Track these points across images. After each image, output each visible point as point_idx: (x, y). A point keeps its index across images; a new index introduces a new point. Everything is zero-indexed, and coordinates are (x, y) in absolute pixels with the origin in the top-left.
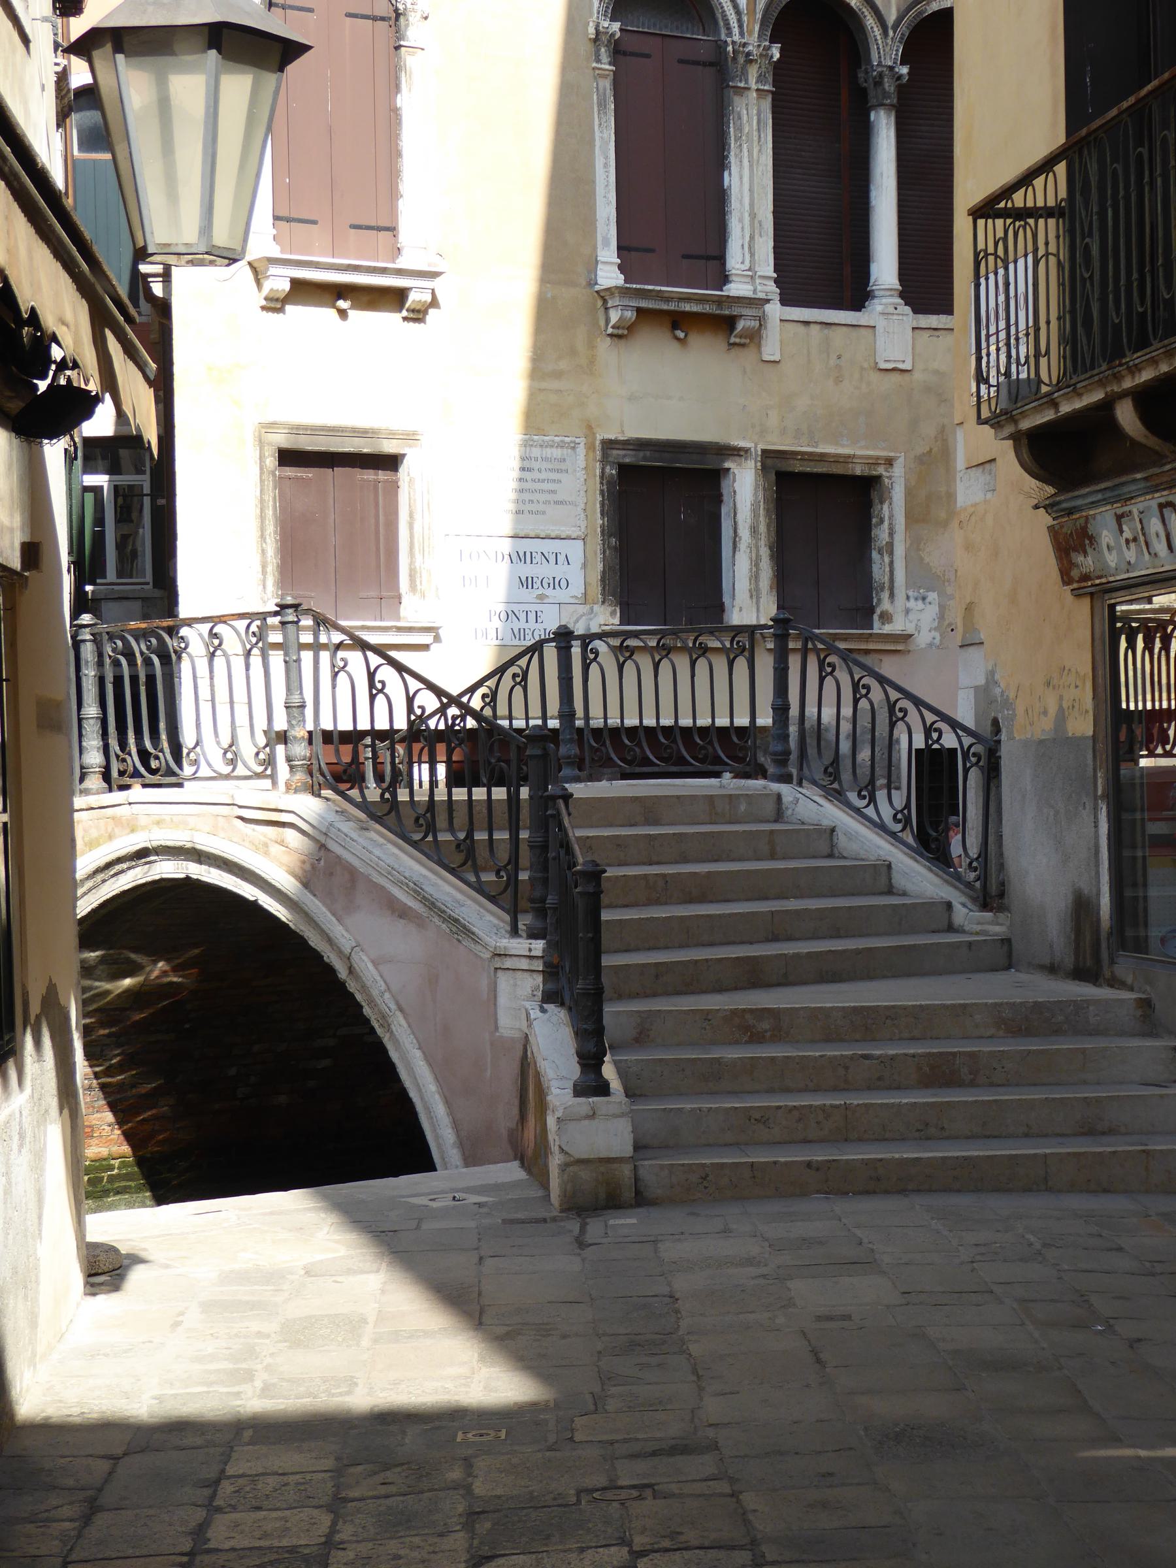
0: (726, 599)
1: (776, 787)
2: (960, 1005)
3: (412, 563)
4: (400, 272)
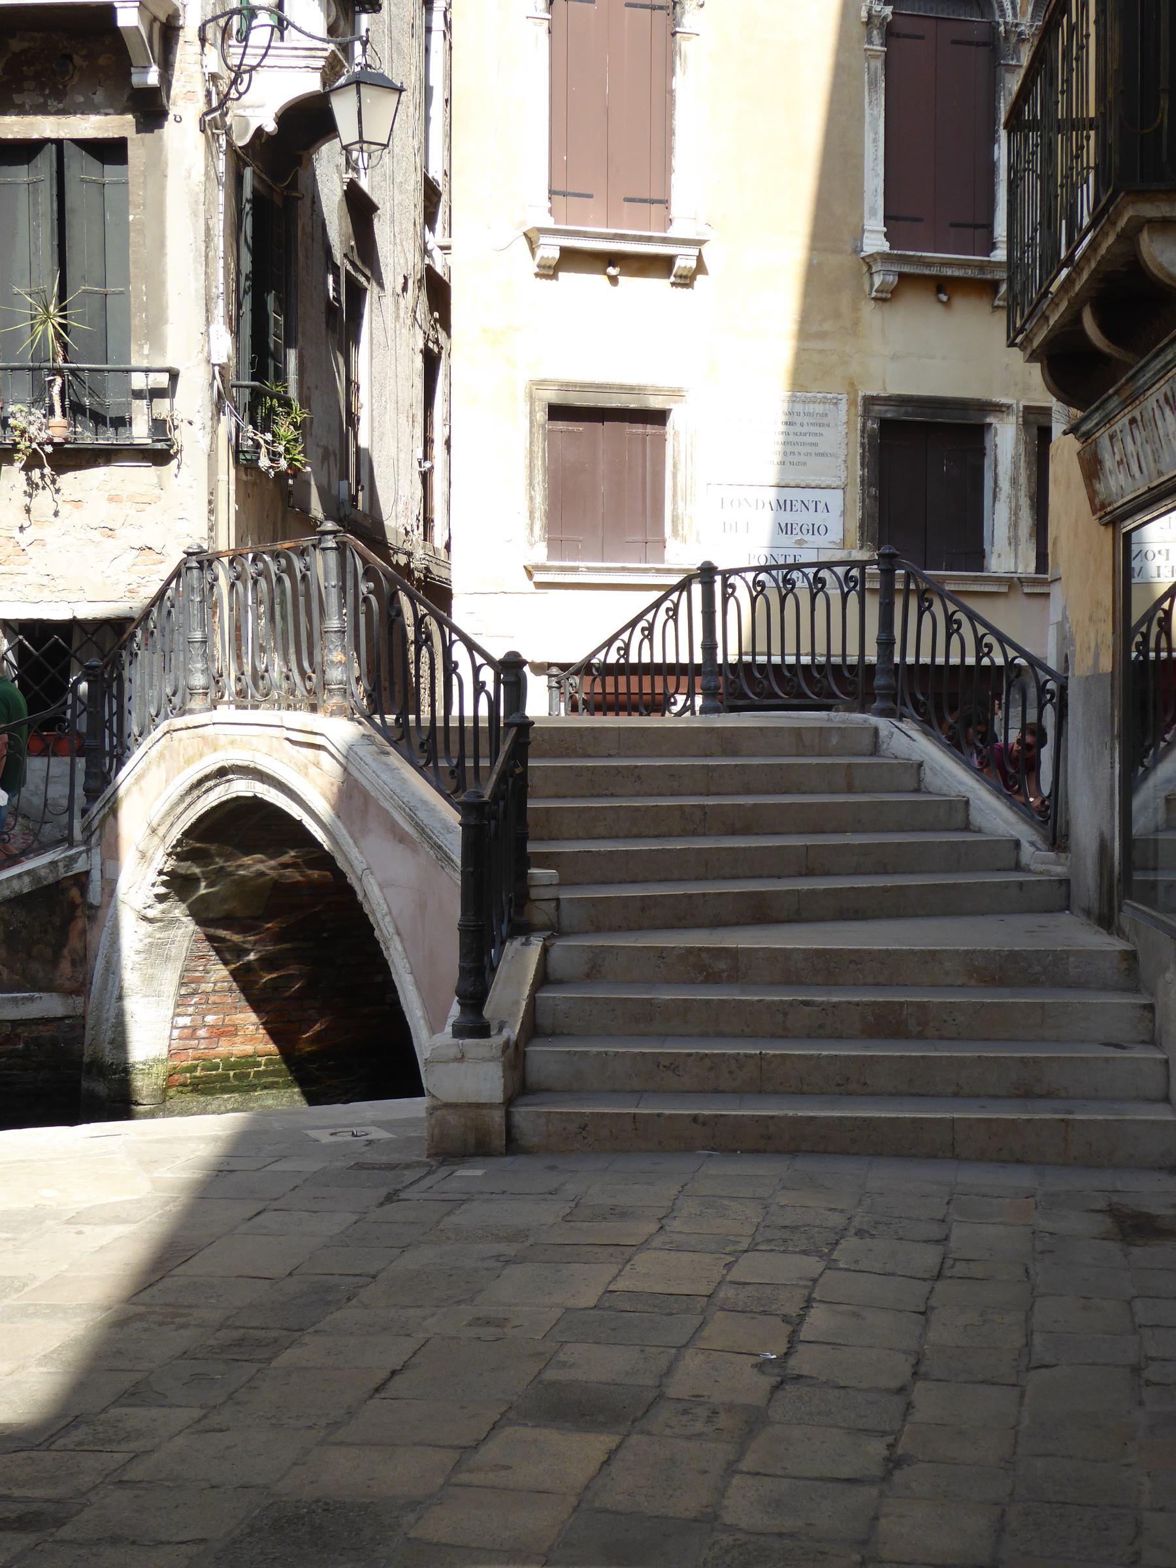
0: (987, 546)
1: (874, 720)
2: (930, 951)
3: (674, 509)
4: (665, 241)
